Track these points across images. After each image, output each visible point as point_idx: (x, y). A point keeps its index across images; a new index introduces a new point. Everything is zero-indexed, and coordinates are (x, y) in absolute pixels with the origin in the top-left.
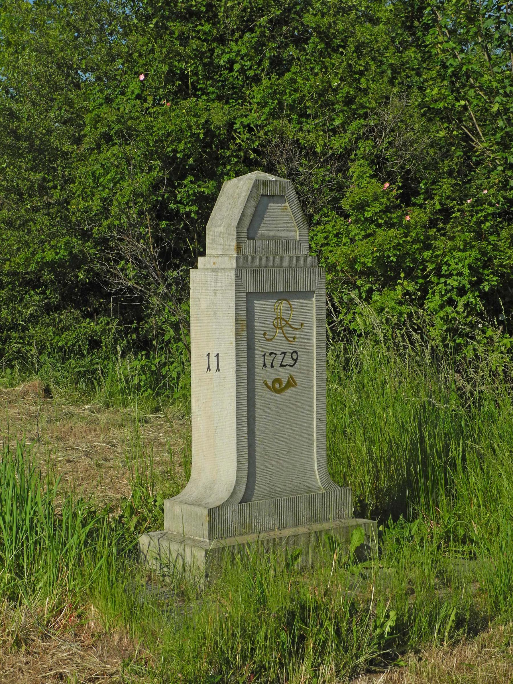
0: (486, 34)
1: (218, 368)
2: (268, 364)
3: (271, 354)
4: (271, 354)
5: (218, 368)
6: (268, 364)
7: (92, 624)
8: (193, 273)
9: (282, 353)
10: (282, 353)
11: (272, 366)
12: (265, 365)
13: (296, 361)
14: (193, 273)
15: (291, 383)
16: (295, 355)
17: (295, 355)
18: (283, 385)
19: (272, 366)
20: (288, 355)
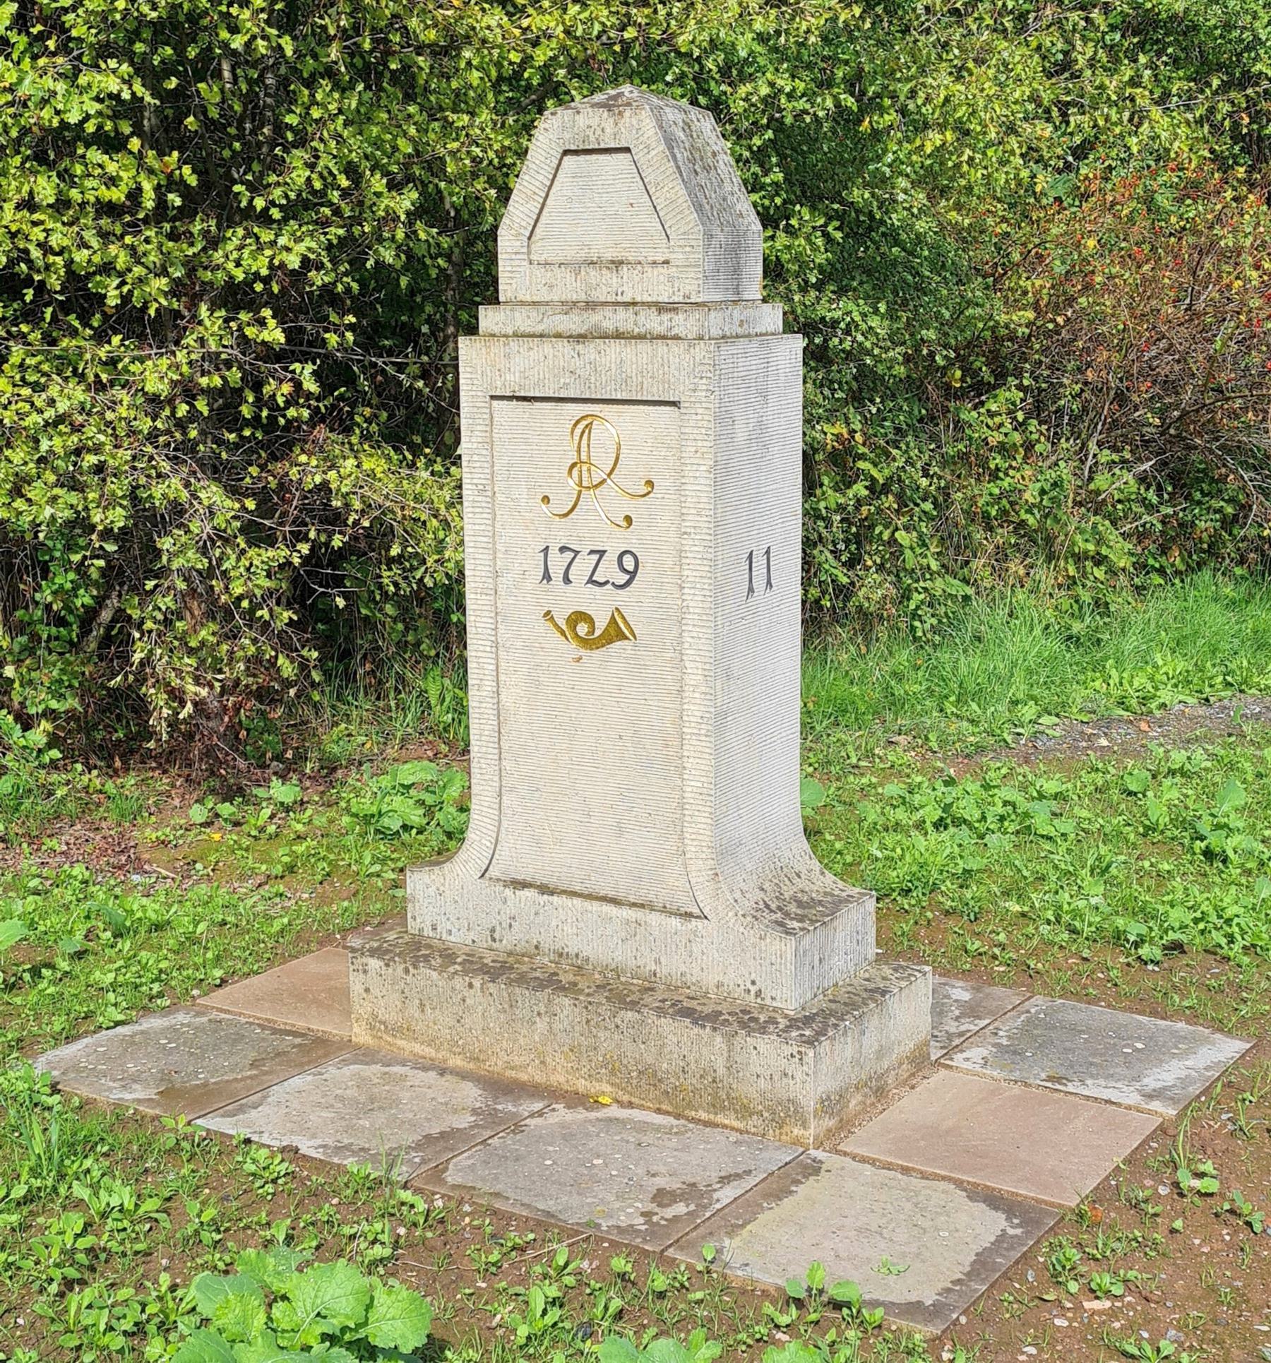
0: (984, 464)
1: (769, 583)
2: (557, 571)
3: (563, 549)
4: (563, 549)
5: (769, 583)
6: (557, 571)
7: (139, 1092)
8: (467, 348)
9: (592, 552)
10: (592, 552)
11: (567, 580)
12: (547, 576)
13: (633, 574)
14: (467, 348)
15: (616, 632)
16: (629, 563)
17: (629, 563)
18: (598, 633)
19: (567, 580)
20: (611, 556)
